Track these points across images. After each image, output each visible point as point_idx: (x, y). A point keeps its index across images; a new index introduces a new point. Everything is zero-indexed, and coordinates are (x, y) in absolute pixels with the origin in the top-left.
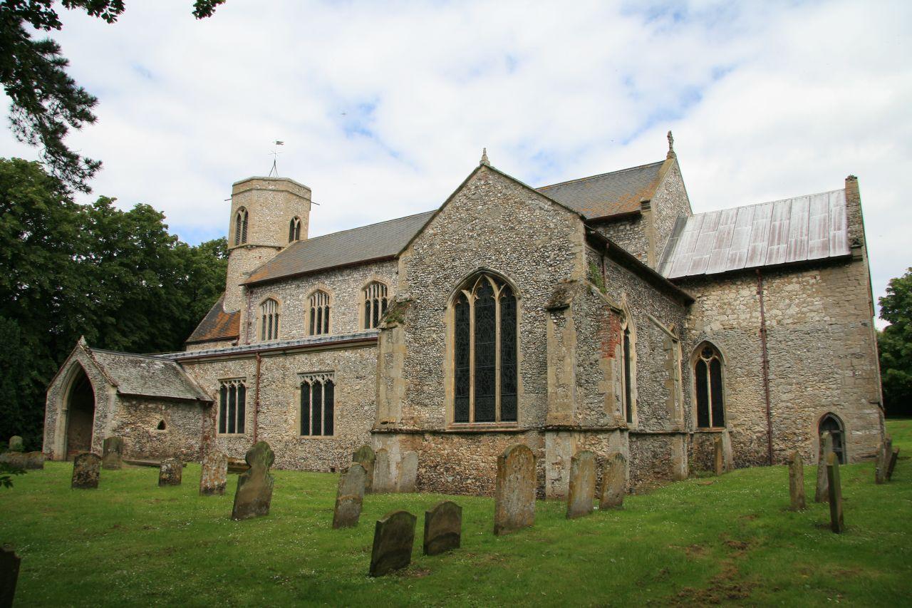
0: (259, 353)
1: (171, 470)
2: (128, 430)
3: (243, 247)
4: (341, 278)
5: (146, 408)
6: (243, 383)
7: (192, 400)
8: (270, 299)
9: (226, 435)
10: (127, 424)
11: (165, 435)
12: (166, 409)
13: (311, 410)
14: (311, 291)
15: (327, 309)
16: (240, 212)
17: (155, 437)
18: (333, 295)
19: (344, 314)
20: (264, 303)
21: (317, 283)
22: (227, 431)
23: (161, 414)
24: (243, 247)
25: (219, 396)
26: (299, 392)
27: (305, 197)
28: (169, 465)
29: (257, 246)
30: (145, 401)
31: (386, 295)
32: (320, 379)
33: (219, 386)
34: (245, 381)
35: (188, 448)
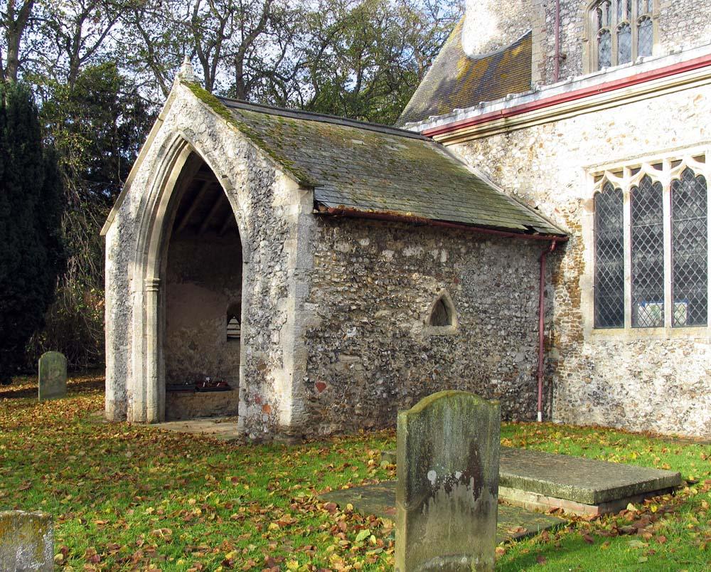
2: (352, 333)
7: (517, 231)
9: (615, 336)
12: (450, 261)
17: (425, 350)
23: (439, 277)
30: (396, 239)
33: (589, 189)
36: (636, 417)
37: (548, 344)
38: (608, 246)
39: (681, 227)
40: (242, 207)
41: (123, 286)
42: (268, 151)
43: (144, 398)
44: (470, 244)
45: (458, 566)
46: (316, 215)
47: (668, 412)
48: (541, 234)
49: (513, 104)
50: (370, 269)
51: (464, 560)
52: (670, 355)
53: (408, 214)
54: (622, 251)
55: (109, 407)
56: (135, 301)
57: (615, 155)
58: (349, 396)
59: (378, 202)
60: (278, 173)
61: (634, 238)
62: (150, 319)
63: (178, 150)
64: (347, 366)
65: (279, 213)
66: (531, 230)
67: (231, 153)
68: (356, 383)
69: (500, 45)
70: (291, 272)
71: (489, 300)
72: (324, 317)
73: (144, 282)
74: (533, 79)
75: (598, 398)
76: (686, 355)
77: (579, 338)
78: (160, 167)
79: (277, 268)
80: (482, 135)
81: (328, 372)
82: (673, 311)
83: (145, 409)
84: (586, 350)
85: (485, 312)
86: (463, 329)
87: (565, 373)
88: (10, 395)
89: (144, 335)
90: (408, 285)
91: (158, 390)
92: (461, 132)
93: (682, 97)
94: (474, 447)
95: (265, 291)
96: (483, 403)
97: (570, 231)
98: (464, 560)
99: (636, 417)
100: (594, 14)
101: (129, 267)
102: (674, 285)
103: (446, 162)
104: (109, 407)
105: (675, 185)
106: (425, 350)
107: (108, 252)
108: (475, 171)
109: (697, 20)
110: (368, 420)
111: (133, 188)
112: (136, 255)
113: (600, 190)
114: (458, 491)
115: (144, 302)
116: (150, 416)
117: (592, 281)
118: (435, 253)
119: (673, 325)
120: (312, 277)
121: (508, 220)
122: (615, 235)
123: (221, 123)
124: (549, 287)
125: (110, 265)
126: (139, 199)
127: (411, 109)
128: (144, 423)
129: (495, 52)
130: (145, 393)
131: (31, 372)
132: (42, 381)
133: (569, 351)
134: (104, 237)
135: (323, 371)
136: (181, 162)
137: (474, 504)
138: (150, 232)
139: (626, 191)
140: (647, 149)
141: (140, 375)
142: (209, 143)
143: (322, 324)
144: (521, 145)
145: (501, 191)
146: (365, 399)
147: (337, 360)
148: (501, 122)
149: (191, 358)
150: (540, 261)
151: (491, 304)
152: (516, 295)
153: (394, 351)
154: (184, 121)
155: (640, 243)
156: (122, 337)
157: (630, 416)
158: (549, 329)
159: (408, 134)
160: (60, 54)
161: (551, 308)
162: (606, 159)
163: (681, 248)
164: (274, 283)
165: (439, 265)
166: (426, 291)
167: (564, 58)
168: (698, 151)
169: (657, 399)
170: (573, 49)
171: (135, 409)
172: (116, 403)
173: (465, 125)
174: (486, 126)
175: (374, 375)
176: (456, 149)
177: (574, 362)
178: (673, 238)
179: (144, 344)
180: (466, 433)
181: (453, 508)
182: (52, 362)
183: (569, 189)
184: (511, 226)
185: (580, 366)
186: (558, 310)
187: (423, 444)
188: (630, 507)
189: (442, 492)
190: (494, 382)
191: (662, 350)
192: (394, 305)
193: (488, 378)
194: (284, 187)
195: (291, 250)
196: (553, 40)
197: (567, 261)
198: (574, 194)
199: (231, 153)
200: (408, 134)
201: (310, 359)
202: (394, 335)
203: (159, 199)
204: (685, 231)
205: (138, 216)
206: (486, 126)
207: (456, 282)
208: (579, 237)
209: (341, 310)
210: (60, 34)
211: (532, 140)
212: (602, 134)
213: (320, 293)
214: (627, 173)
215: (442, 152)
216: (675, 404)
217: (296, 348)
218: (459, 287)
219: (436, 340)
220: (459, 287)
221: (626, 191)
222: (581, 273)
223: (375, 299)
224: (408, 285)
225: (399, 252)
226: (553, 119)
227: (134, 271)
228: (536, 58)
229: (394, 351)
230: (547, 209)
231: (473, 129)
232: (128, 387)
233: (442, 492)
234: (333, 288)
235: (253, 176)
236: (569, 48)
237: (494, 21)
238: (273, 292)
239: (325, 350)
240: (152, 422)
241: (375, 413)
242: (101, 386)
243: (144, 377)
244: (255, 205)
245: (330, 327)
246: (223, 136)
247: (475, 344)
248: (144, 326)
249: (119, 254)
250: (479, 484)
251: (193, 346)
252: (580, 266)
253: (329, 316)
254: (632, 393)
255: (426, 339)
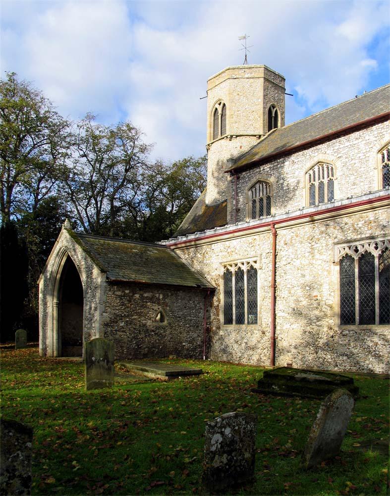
0: (274, 224)
1: (233, 442)
2: (122, 324)
3: (223, 138)
4: (347, 144)
5: (142, 297)
6: (253, 264)
7: (192, 287)
8: (259, 182)
9: (232, 327)
10: (122, 317)
11: (164, 328)
12: (164, 298)
13: (357, 291)
14: (309, 165)
15: (331, 182)
16: (217, 106)
17: (153, 331)
18: (338, 165)
19: (354, 184)
20: (253, 186)
21: (316, 154)
22: (377, 319)
23: (159, 304)
24: (223, 138)
25: (221, 282)
26: (338, 268)
27: (281, 85)
28: (228, 431)
29: (237, 136)
30: (140, 290)
31: (333, 176)
32: (371, 249)
33: (222, 271)
34: (255, 262)
35: (190, 342)
36: (236, 358)
37: (208, 330)
38: (228, 293)
39: (250, 287)
40: (84, 277)
41: (45, 304)
42: (91, 258)
43: (53, 347)
44: (173, 292)
45: (102, 382)
46: (107, 282)
47: (246, 356)
48: (204, 288)
49: (197, 236)
50: (130, 301)
51: (104, 381)
52: (247, 335)
53: (144, 281)
54: (354, 287)
55: (40, 351)
56: (50, 310)
57: (230, 259)
58: (122, 347)
59: (133, 276)
60: (95, 266)
61: (236, 290)
62: (50, 316)
63: (64, 254)
64: (120, 336)
65: (95, 280)
66: (199, 286)
67: (80, 258)
68: (125, 343)
69: (219, 201)
70: (98, 302)
71: (181, 313)
72: (111, 318)
73: (53, 303)
74: (228, 218)
75: (225, 351)
76: (251, 334)
77: (219, 328)
78: (57, 260)
79: (94, 300)
80: (187, 247)
81: (112, 338)
82: (248, 318)
83: (53, 353)
84: (221, 333)
85: (179, 317)
86: (170, 324)
87: (214, 341)
88: (6, 348)
89: (53, 323)
90: (146, 307)
91: (58, 344)
92: (179, 246)
93: (250, 239)
94: (106, 352)
95: (90, 308)
96: (108, 342)
97: (216, 287)
98: (104, 381)
99: (236, 358)
100: (250, 193)
101: (47, 297)
102: (248, 309)
103: (173, 258)
104: (40, 351)
105: (248, 271)
106: (153, 331)
107: (40, 291)
108: (184, 261)
109: (286, 199)
110: (129, 356)
111: (49, 266)
112: (50, 292)
113: (225, 272)
114: (102, 363)
115: (53, 310)
116: (55, 354)
117: (223, 306)
118: (157, 295)
119: (248, 323)
120: (105, 304)
121: (189, 283)
122: (230, 289)
123: (77, 247)
124: (209, 308)
125: (41, 295)
126: (50, 271)
127: (181, 227)
128: (53, 357)
129: (217, 204)
130: (53, 345)
131: (12, 339)
132: (17, 342)
133: (216, 333)
134: (38, 285)
135: (111, 337)
136: (65, 259)
137: (106, 367)
138: (55, 284)
139: (233, 272)
140: (239, 257)
141: (51, 339)
142: (73, 253)
143: (110, 321)
144: (200, 252)
145: (193, 270)
146: (128, 348)
147: (116, 334)
148: (193, 243)
149: (73, 333)
150: (205, 298)
151: (182, 315)
152: (194, 311)
153: (140, 331)
154: (65, 243)
155: (238, 292)
156: (45, 324)
157: (235, 357)
158: (209, 325)
159: (160, 246)
160: (31, 195)
161: (210, 316)
162: (227, 259)
163: (250, 295)
164: (93, 305)
165: (159, 299)
166: (153, 309)
167: (239, 210)
168: (255, 259)
169: (243, 351)
170: (242, 206)
171: (49, 351)
172: (43, 349)
173: (181, 243)
174: (188, 244)
175: (132, 340)
176: (178, 252)
177: (217, 337)
178: (248, 291)
179: (53, 327)
180: (103, 348)
181: (100, 367)
182: (21, 333)
183: (216, 271)
184: (189, 285)
185: (219, 339)
186: (212, 318)
187: (90, 350)
188: (180, 377)
189: (96, 363)
190: (184, 344)
191: (244, 333)
192: (140, 314)
193: (181, 343)
194: (96, 271)
195: (98, 294)
196: (234, 202)
197: (215, 298)
198: (217, 273)
199: (80, 258)
200: (160, 246)
201: (105, 333)
202: (140, 325)
203: (58, 271)
204: (251, 289)
205: (50, 277)
206: (188, 244)
207: (166, 306)
208: (219, 289)
209: (118, 316)
210: (31, 186)
211: (204, 251)
212: (226, 250)
213: (109, 310)
214: (233, 265)
215: (173, 253)
216: (248, 353)
217: (100, 329)
218: (168, 308)
219: (158, 328)
220: (168, 308)
221: (233, 272)
222: (219, 303)
223: (132, 312)
224: (146, 307)
225: (142, 295)
226: (211, 243)
227: (49, 299)
228: (229, 209)
229: (140, 331)
230: (208, 277)
231: (183, 245)
232: (47, 343)
233: (96, 363)
234: (114, 308)
235: (87, 266)
236: (241, 206)
237: (216, 190)
238: (93, 309)
239: (112, 330)
240: (56, 357)
241: (132, 354)
242: (38, 345)
243: (53, 340)
244: (87, 277)
245: (113, 322)
246: (77, 250)
247: (175, 329)
248: (53, 320)
249: (44, 292)
250: (108, 362)
251: (74, 328)
252: (219, 301)
253: (113, 318)
254: (235, 349)
255: (153, 327)
